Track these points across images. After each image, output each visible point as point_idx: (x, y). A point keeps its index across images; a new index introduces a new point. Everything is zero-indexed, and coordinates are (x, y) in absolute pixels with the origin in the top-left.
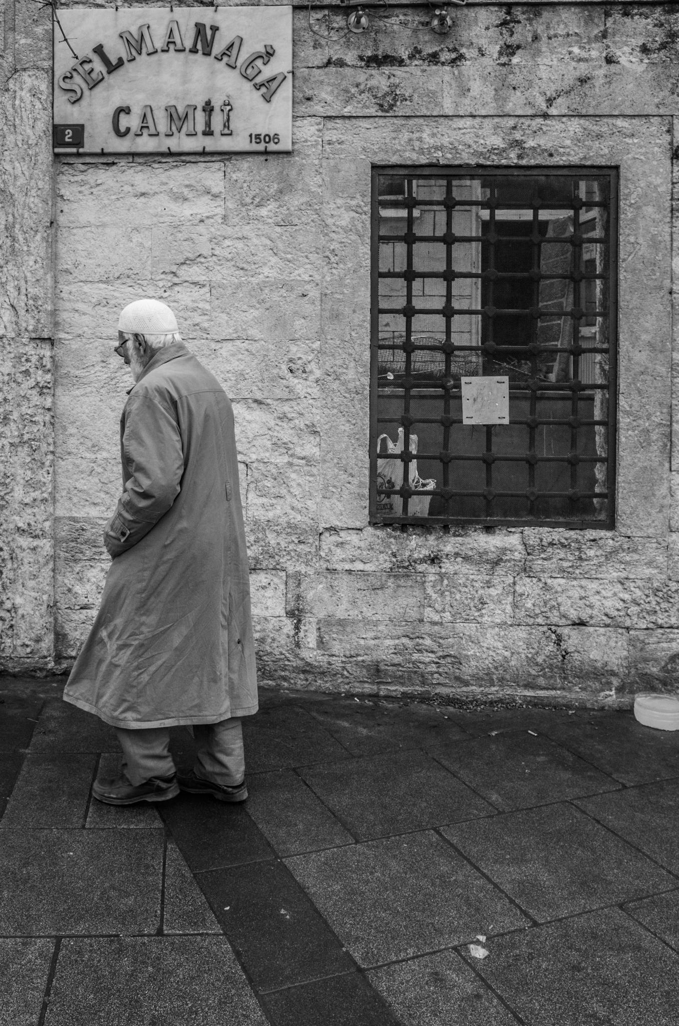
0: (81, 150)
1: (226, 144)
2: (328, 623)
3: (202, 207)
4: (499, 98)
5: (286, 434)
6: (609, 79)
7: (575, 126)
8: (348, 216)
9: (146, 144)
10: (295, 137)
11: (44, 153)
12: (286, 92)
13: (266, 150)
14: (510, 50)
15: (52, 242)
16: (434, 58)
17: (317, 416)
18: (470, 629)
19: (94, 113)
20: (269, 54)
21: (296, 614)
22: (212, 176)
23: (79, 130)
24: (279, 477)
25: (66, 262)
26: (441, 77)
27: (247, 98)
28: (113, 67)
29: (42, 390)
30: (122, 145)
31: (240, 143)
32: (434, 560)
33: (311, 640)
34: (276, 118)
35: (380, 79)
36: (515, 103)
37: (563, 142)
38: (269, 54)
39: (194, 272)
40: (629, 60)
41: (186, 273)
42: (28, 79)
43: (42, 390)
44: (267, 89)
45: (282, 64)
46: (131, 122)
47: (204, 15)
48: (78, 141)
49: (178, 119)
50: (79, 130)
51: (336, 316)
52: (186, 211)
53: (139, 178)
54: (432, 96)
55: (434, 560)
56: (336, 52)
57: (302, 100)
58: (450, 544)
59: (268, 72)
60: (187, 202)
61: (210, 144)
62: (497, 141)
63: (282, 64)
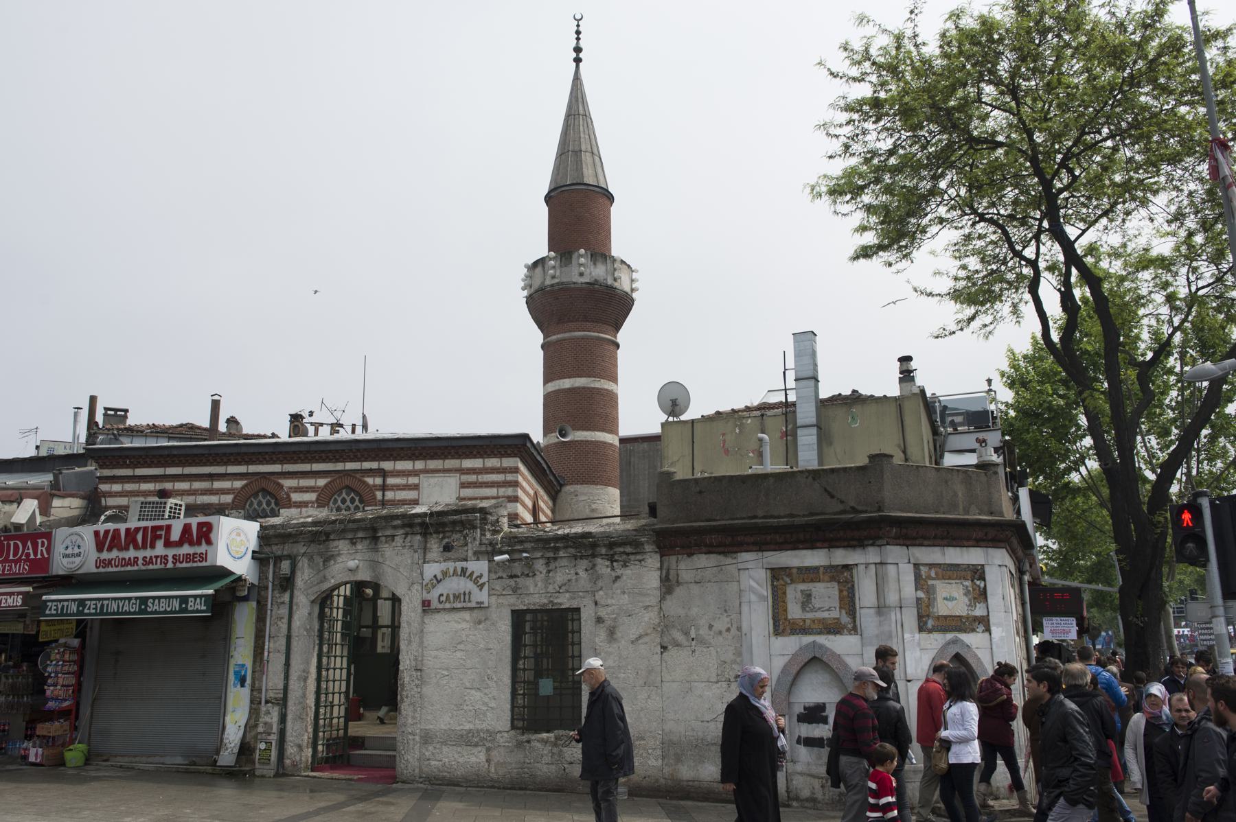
0: (142, 499)
1: (469, 605)
2: (498, 763)
3: (464, 625)
4: (546, 587)
5: (486, 700)
6: (577, 580)
7: (567, 595)
8: (504, 627)
9: (448, 606)
10: (861, 568)
11: (420, 609)
12: (486, 588)
13: (480, 607)
14: (549, 571)
15: (421, 638)
16: (527, 575)
17: (495, 693)
18: (538, 765)
19: (433, 596)
20: (481, 576)
21: (488, 761)
22: (466, 615)
23: (429, 602)
24: (485, 715)
25: (426, 644)
26: (529, 582)
27: (475, 589)
28: (439, 582)
29: (417, 686)
30: (441, 606)
31: (473, 605)
32: (528, 742)
33: (493, 770)
34: (482, 596)
35: (512, 582)
36: (551, 589)
37: (565, 601)
38: (481, 576)
39: (461, 647)
40: (582, 574)
41: (459, 647)
42: (415, 586)
43: (417, 686)
44: (481, 587)
45: (485, 579)
46: (443, 599)
47: (464, 564)
48: (429, 605)
49: (456, 597)
50: (429, 602)
51: (501, 660)
52: (460, 626)
53: (447, 617)
54: (527, 588)
55: (528, 742)
56: (500, 574)
57: (491, 589)
58: (533, 737)
59: (481, 581)
60: (458, 624)
61: (465, 605)
62: (546, 601)
63: (485, 579)
